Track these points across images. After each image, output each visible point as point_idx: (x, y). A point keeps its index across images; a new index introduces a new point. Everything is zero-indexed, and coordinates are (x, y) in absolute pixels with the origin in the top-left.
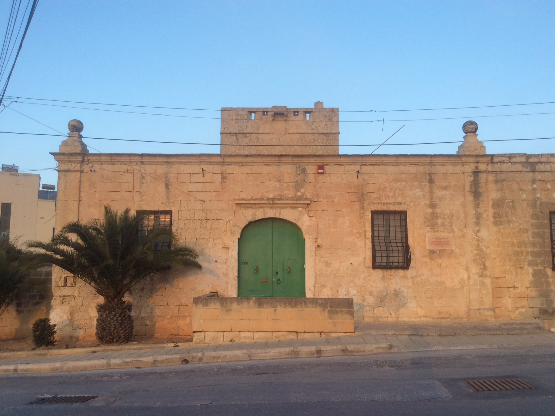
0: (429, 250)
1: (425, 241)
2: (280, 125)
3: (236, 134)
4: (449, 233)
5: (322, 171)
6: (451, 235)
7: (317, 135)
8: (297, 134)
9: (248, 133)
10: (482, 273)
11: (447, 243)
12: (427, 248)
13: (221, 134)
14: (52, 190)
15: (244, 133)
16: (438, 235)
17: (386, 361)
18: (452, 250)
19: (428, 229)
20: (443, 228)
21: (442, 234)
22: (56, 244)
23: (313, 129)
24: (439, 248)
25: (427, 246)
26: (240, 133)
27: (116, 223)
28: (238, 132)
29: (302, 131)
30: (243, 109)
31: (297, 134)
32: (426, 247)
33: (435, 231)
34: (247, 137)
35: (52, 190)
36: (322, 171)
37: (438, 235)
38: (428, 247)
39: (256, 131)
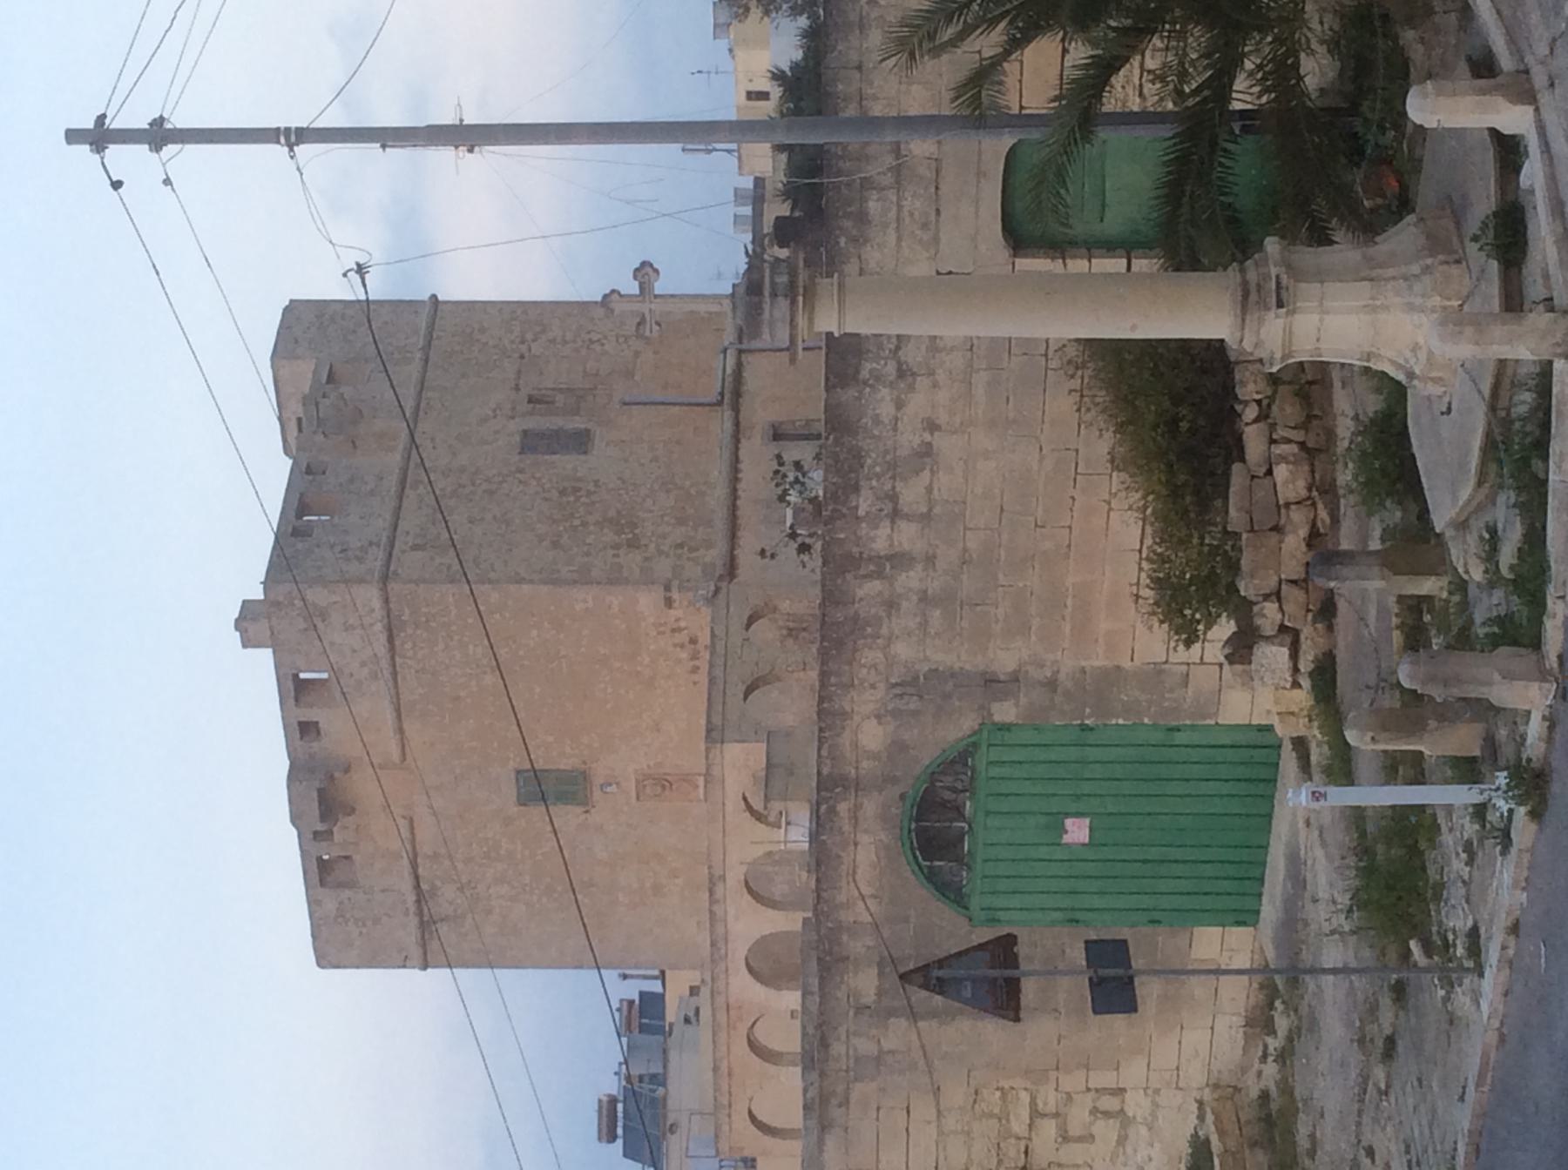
2: (363, 786)
3: (423, 925)
7: (398, 659)
8: (400, 498)
9: (417, 886)
10: (858, 786)
13: (425, 967)
14: (620, 1107)
15: (418, 901)
17: (1482, 651)
22: (1550, 672)
23: (374, 676)
26: (420, 914)
28: (413, 921)
29: (389, 715)
30: (313, 903)
31: (401, 731)
34: (434, 888)
35: (620, 1107)
39: (405, 862)
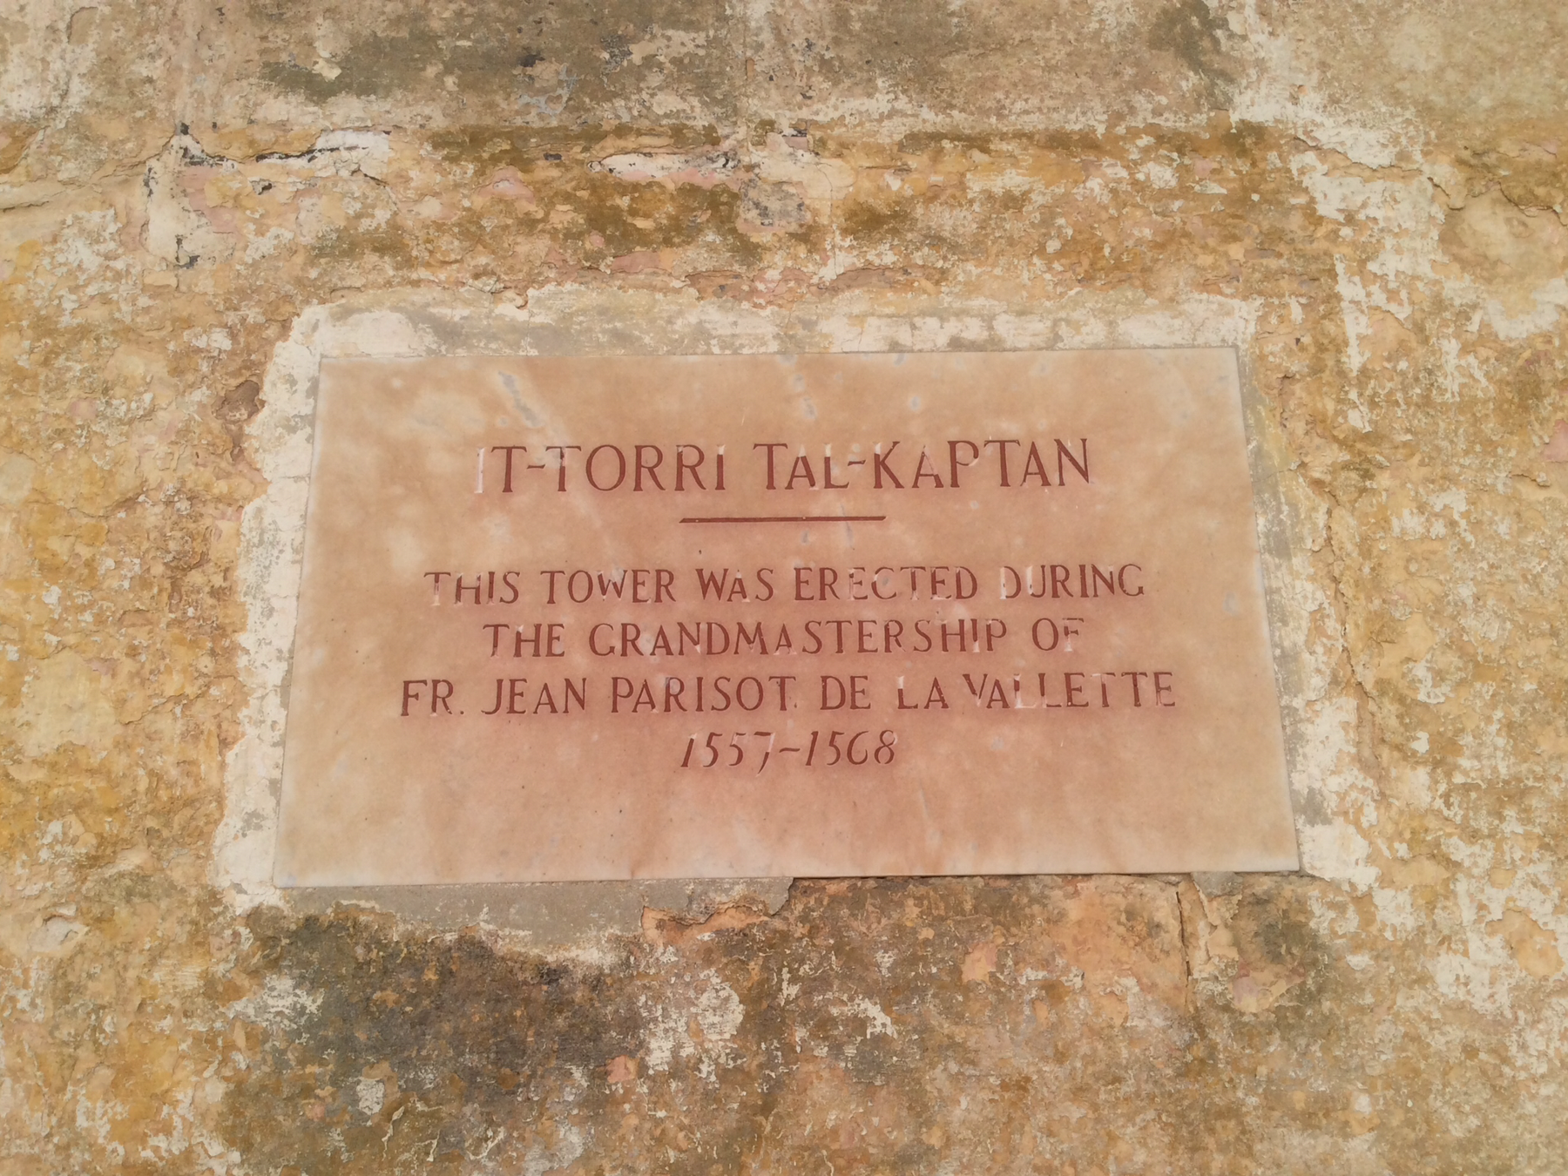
0: (308, 939)
1: (190, 588)
4: (1097, 262)
5: (834, 701)
6: (1197, 335)
11: (1069, 639)
12: (251, 871)
16: (700, 343)
18: (1275, 924)
19: (371, 147)
20: (880, 109)
21: (854, 331)
24: (737, 846)
25: (253, 766)
27: (576, 943)
32: (185, 817)
33: (612, 227)
36: (834, 701)
37: (700, 343)
38: (304, 808)
